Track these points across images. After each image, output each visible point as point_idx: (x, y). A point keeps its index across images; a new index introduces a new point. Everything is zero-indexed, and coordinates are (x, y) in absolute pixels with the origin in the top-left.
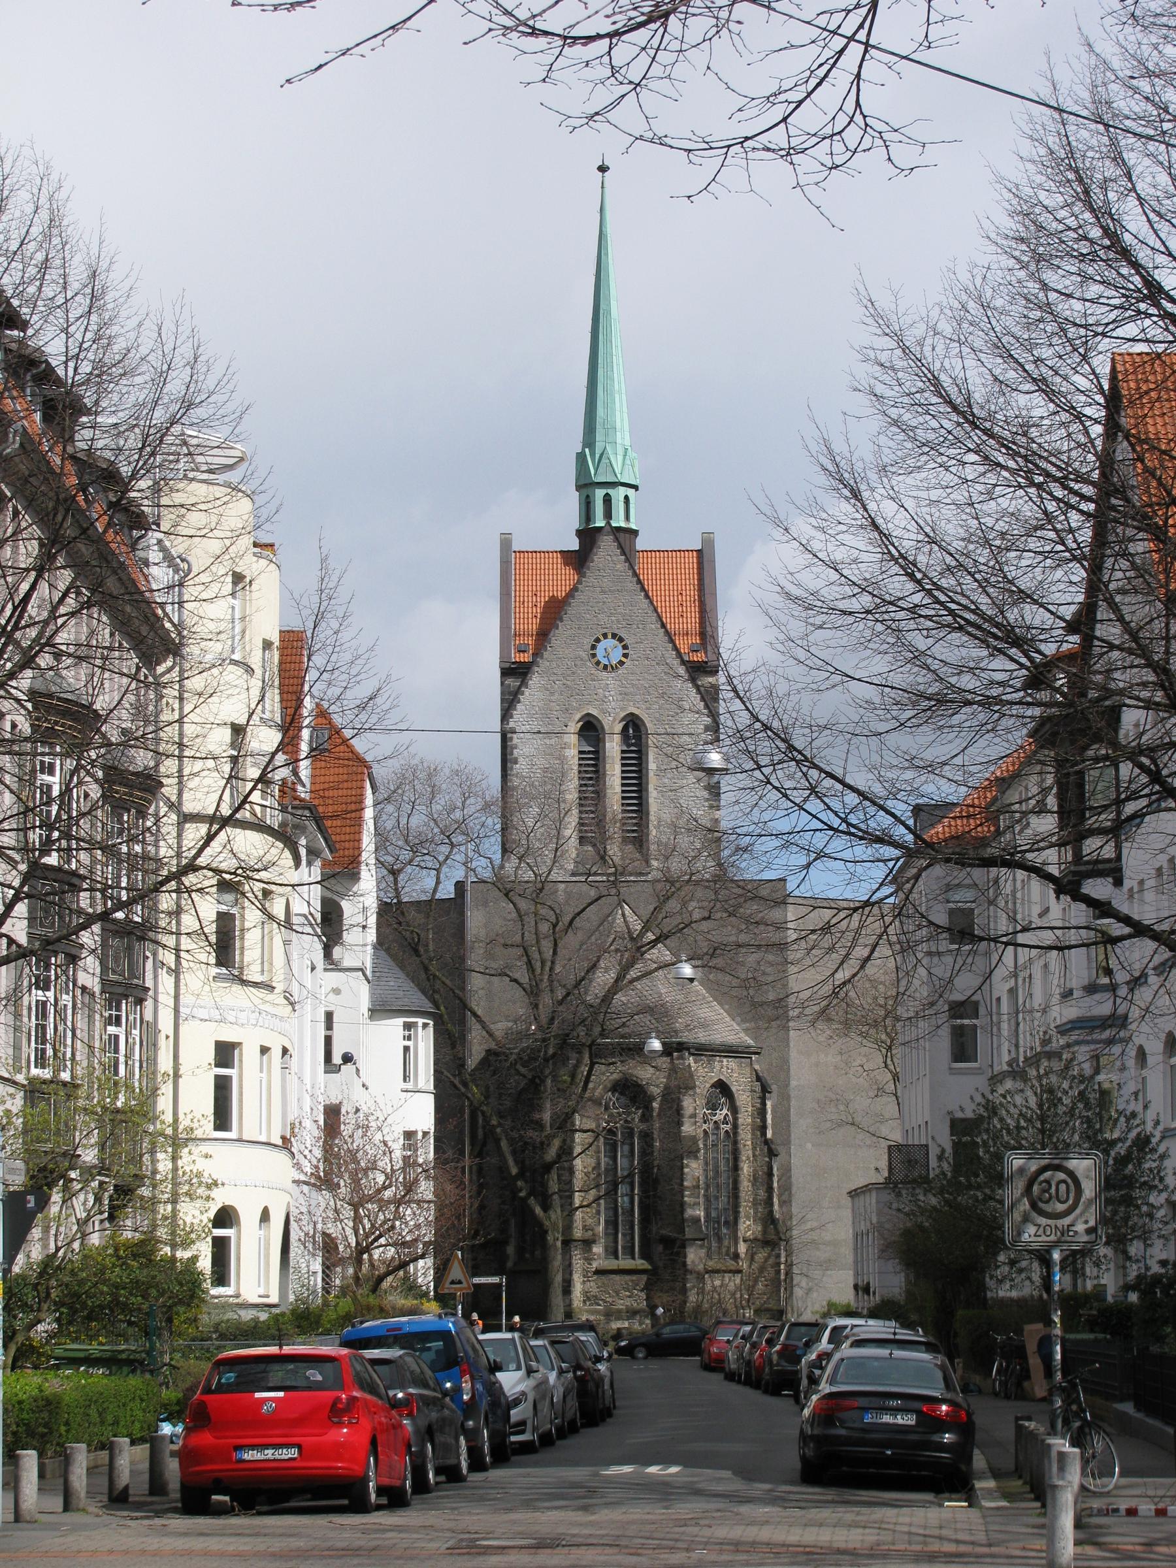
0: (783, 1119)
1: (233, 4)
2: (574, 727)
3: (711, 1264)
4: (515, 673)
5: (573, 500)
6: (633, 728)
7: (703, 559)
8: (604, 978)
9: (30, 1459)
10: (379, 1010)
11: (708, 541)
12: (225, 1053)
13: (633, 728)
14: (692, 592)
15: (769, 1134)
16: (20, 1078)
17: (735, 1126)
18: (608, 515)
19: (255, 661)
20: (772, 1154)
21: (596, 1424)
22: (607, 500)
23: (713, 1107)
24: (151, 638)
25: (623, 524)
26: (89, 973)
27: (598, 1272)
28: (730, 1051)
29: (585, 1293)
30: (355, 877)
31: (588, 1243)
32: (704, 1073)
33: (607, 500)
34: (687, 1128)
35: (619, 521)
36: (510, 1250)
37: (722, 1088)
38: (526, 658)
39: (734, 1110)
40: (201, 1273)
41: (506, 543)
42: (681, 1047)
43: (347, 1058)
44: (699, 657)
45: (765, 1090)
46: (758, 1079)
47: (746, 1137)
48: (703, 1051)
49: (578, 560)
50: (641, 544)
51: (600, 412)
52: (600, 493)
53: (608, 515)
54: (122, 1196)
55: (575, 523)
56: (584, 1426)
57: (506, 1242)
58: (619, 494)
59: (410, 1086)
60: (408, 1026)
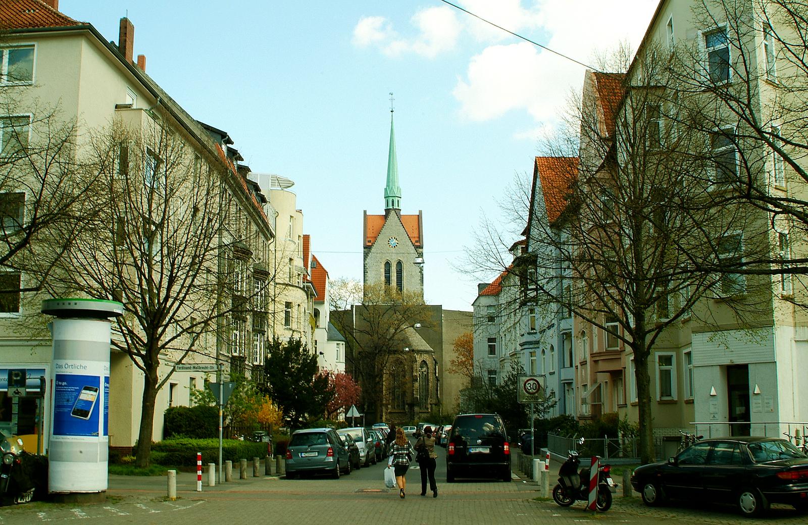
0: (441, 371)
1: (291, 217)
2: (383, 264)
3: (421, 411)
4: (367, 248)
5: (384, 201)
6: (399, 264)
7: (419, 217)
8: (392, 331)
9: (230, 464)
10: (330, 339)
11: (420, 212)
12: (288, 305)
13: (399, 264)
14: (416, 226)
15: (437, 375)
16: (230, 356)
17: (428, 373)
18: (393, 205)
19: (297, 241)
20: (438, 380)
21: (381, 461)
22: (393, 202)
23: (422, 367)
24: (266, 232)
25: (397, 208)
26: (249, 325)
27: (390, 413)
28: (426, 352)
29: (386, 418)
30: (323, 303)
31: (386, 405)
32: (419, 359)
33: (393, 202)
34: (415, 374)
35: (396, 207)
36: (366, 407)
37: (424, 362)
38: (370, 244)
39: (428, 368)
40: (283, 459)
41: (365, 212)
42: (413, 350)
43: (321, 353)
44: (418, 244)
45: (436, 363)
46: (434, 360)
47: (431, 377)
48: (420, 352)
49: (386, 217)
50: (402, 213)
51: (391, 177)
52: (390, 199)
53: (393, 205)
54: (242, 308)
55: (384, 207)
56: (378, 461)
57: (364, 405)
58: (396, 200)
59: (337, 361)
60: (338, 344)
